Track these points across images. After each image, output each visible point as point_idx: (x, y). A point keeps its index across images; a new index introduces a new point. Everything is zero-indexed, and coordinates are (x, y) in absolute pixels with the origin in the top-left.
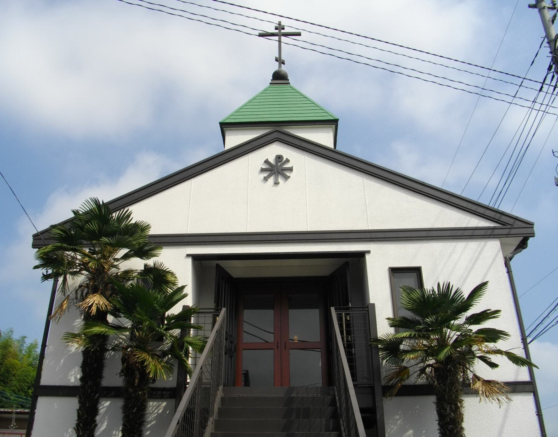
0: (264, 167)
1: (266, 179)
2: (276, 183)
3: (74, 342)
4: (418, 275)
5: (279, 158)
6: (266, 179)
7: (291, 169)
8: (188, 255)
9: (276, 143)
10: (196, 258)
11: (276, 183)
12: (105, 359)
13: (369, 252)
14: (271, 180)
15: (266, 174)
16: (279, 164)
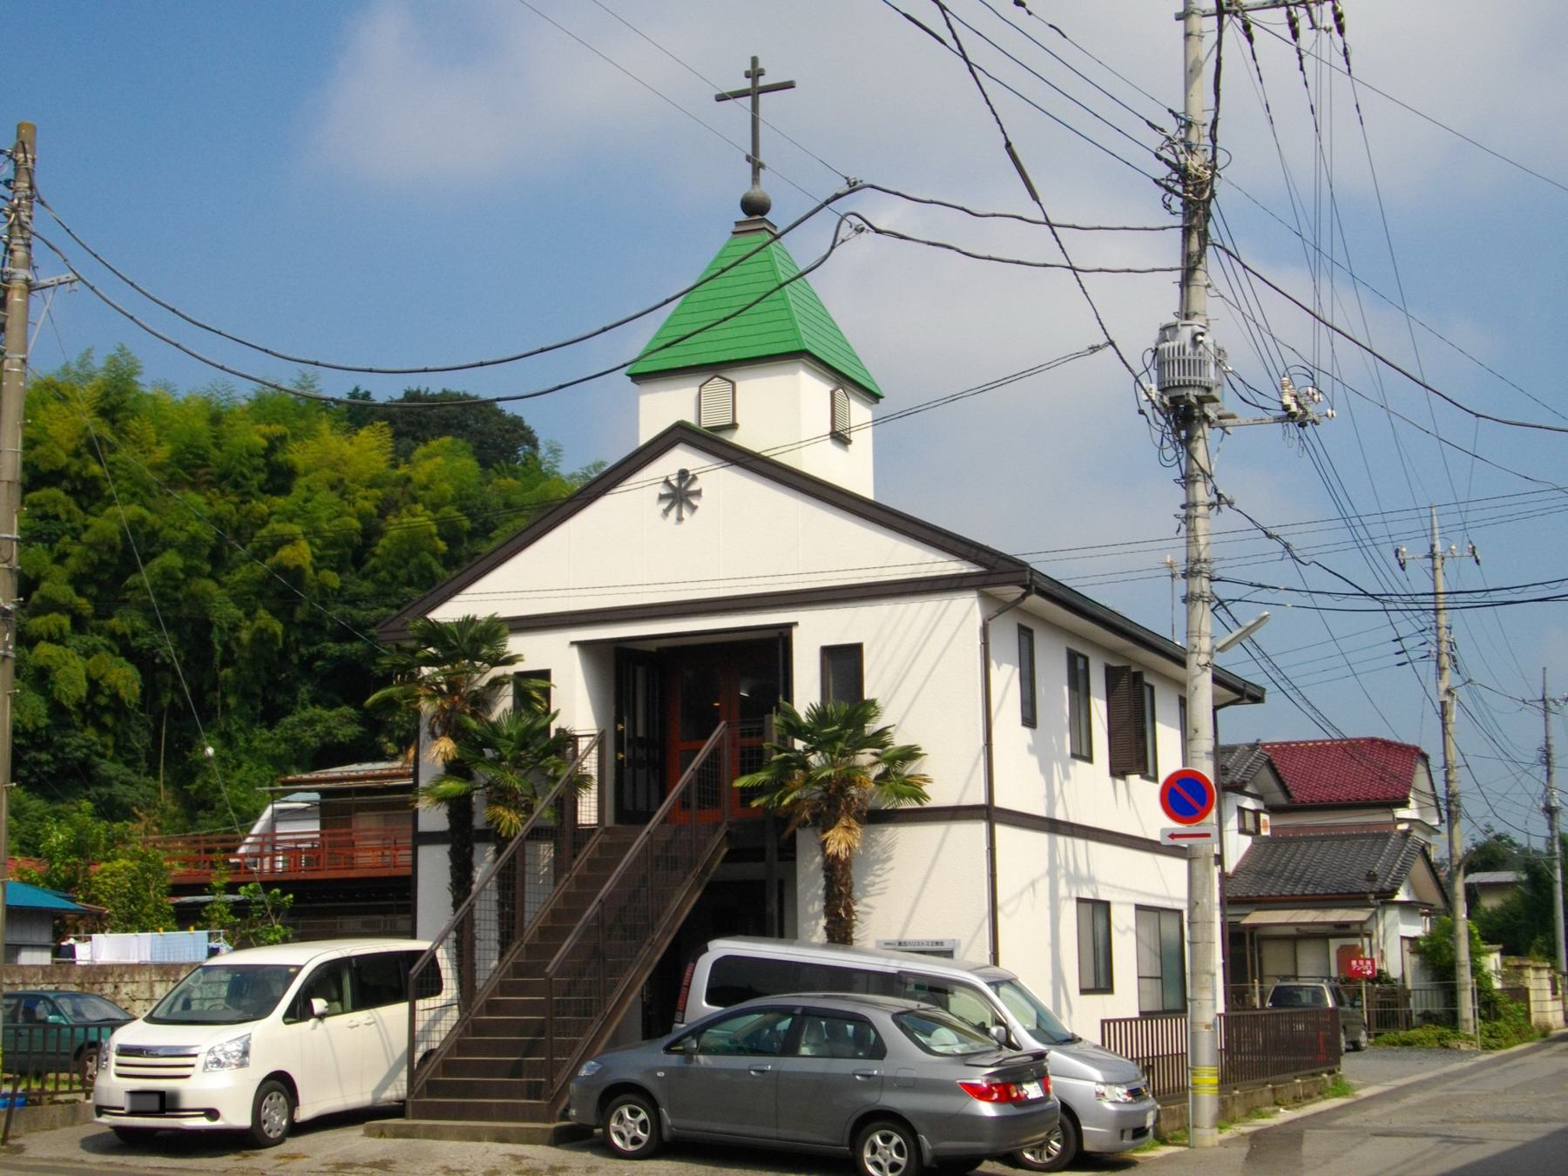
0: (664, 492)
1: (666, 512)
2: (694, 508)
3: (1268, 747)
4: (394, 771)
5: (683, 474)
6: (666, 512)
7: (698, 493)
8: (573, 643)
9: (681, 446)
10: (583, 645)
11: (680, 519)
12: (1507, 903)
13: (796, 624)
14: (673, 513)
15: (665, 505)
16: (683, 485)
